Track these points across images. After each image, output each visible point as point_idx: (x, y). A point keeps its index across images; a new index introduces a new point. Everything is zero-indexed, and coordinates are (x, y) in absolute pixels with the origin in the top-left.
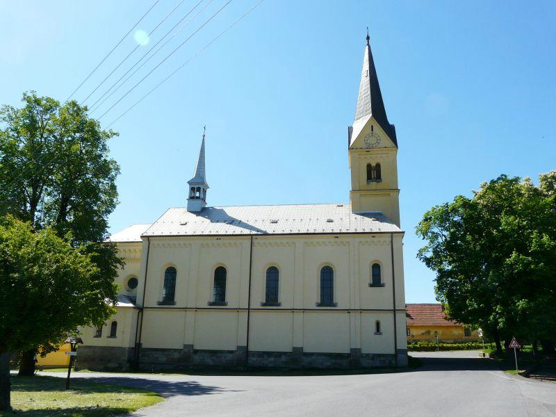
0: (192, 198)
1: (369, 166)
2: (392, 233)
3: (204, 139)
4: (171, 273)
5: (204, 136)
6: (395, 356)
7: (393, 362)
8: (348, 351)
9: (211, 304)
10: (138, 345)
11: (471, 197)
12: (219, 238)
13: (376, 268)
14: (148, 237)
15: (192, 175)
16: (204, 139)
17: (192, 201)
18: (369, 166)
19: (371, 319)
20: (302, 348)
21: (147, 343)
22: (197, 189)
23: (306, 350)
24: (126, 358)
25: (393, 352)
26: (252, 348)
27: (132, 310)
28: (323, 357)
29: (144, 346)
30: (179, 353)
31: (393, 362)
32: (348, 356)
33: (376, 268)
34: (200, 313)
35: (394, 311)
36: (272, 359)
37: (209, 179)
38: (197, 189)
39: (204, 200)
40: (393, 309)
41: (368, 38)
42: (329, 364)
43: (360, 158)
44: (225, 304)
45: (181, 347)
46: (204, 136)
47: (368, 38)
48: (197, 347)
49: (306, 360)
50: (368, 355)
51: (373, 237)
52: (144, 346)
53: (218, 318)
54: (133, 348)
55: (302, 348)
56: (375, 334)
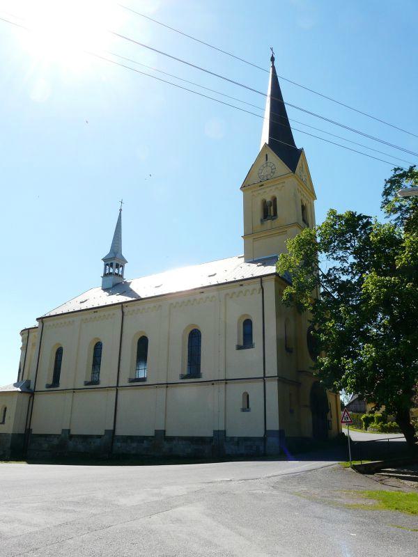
0: (105, 275)
1: (264, 202)
2: (261, 277)
3: (120, 214)
4: (59, 353)
5: (121, 210)
6: (264, 439)
7: (262, 448)
8: (210, 434)
9: (183, 377)
10: (28, 430)
11: (315, 201)
12: (95, 310)
13: (248, 324)
14: (40, 318)
15: (106, 251)
16: (120, 214)
17: (106, 278)
18: (264, 202)
19: (236, 391)
20: (165, 431)
21: (37, 429)
22: (114, 261)
23: (168, 434)
24: (9, 445)
25: (261, 434)
26: (119, 432)
27: (17, 395)
28: (184, 442)
29: (34, 432)
30: (58, 438)
31: (262, 448)
32: (211, 439)
33: (248, 324)
34: (79, 395)
35: (264, 378)
36: (134, 445)
37: (126, 252)
38: (114, 261)
39: (121, 276)
40: (116, 385)
41: (273, 59)
42: (189, 450)
43: (253, 195)
44: (58, 386)
45: (60, 433)
46: (121, 210)
47: (273, 59)
48: (73, 432)
49: (166, 446)
50: (232, 438)
51: (242, 285)
52: (34, 432)
53: (188, 393)
54: (19, 435)
55: (165, 431)
56: (243, 410)
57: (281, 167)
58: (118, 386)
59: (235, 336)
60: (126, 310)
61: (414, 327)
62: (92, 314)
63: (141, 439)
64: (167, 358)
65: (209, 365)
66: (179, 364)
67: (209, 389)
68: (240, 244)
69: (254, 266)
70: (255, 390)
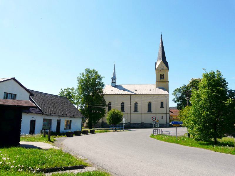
0: (112, 82)
1: (161, 75)
6: (166, 124)
19: (160, 116)
25: (166, 123)
35: (166, 113)
41: (161, 35)
47: (161, 35)
49: (145, 125)
57: (164, 64)
58: (130, 113)
59: (160, 105)
60: (132, 96)
61: (42, 95)
62: (121, 96)
63: (138, 124)
64: (143, 107)
65: (153, 110)
66: (146, 109)
67: (140, 115)
68: (155, 83)
69: (160, 90)
70: (164, 116)
